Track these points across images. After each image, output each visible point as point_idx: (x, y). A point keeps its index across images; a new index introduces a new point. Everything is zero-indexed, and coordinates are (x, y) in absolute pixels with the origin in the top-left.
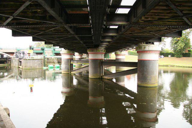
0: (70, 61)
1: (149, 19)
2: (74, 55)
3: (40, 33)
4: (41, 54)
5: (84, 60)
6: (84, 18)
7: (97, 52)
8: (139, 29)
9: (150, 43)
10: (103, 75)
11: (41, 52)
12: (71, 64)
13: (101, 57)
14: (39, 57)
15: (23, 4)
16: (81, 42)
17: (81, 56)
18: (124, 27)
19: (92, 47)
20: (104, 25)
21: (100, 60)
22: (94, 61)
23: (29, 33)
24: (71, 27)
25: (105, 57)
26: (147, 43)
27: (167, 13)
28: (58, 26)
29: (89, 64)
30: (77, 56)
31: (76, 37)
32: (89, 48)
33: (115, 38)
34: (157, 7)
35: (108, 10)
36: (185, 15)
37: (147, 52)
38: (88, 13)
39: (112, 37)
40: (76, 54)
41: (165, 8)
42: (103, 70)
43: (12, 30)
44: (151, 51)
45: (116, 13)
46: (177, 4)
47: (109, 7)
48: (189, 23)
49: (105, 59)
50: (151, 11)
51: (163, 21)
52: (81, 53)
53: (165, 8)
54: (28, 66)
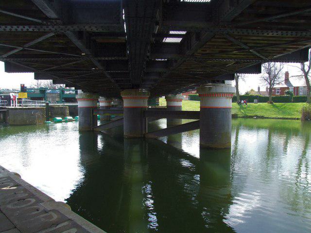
0: (93, 110)
1: (208, 52)
2: (98, 101)
3: (52, 68)
4: (40, 99)
5: (115, 109)
6: (123, 46)
7: (136, 95)
8: (196, 63)
9: (218, 81)
10: (147, 132)
11: (41, 96)
12: (93, 116)
13: (145, 104)
14: (37, 105)
15: (45, 35)
16: (113, 80)
17: (110, 102)
18: (176, 61)
19: (128, 88)
20: (148, 57)
21: (142, 108)
22: (132, 110)
23: (35, 68)
24: (99, 61)
25: (149, 104)
26: (213, 82)
27: (229, 46)
28: (47, 29)
29: (124, 115)
30: (102, 103)
31: (113, 80)
32: (123, 89)
33: (165, 74)
34: (213, 40)
35: (153, 39)
36: (251, 48)
37: (213, 96)
38: (124, 41)
39: (160, 74)
40: (101, 99)
41: (224, 40)
42: (147, 124)
43: (4, 62)
44: (220, 93)
45: (164, 41)
46: (236, 37)
47: (154, 35)
48: (264, 58)
49: (150, 107)
50: (208, 44)
51: (227, 54)
52: (108, 96)
53: (224, 40)
54: (123, 92)
